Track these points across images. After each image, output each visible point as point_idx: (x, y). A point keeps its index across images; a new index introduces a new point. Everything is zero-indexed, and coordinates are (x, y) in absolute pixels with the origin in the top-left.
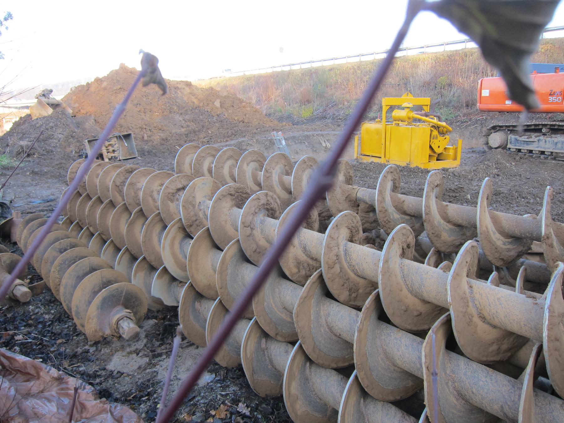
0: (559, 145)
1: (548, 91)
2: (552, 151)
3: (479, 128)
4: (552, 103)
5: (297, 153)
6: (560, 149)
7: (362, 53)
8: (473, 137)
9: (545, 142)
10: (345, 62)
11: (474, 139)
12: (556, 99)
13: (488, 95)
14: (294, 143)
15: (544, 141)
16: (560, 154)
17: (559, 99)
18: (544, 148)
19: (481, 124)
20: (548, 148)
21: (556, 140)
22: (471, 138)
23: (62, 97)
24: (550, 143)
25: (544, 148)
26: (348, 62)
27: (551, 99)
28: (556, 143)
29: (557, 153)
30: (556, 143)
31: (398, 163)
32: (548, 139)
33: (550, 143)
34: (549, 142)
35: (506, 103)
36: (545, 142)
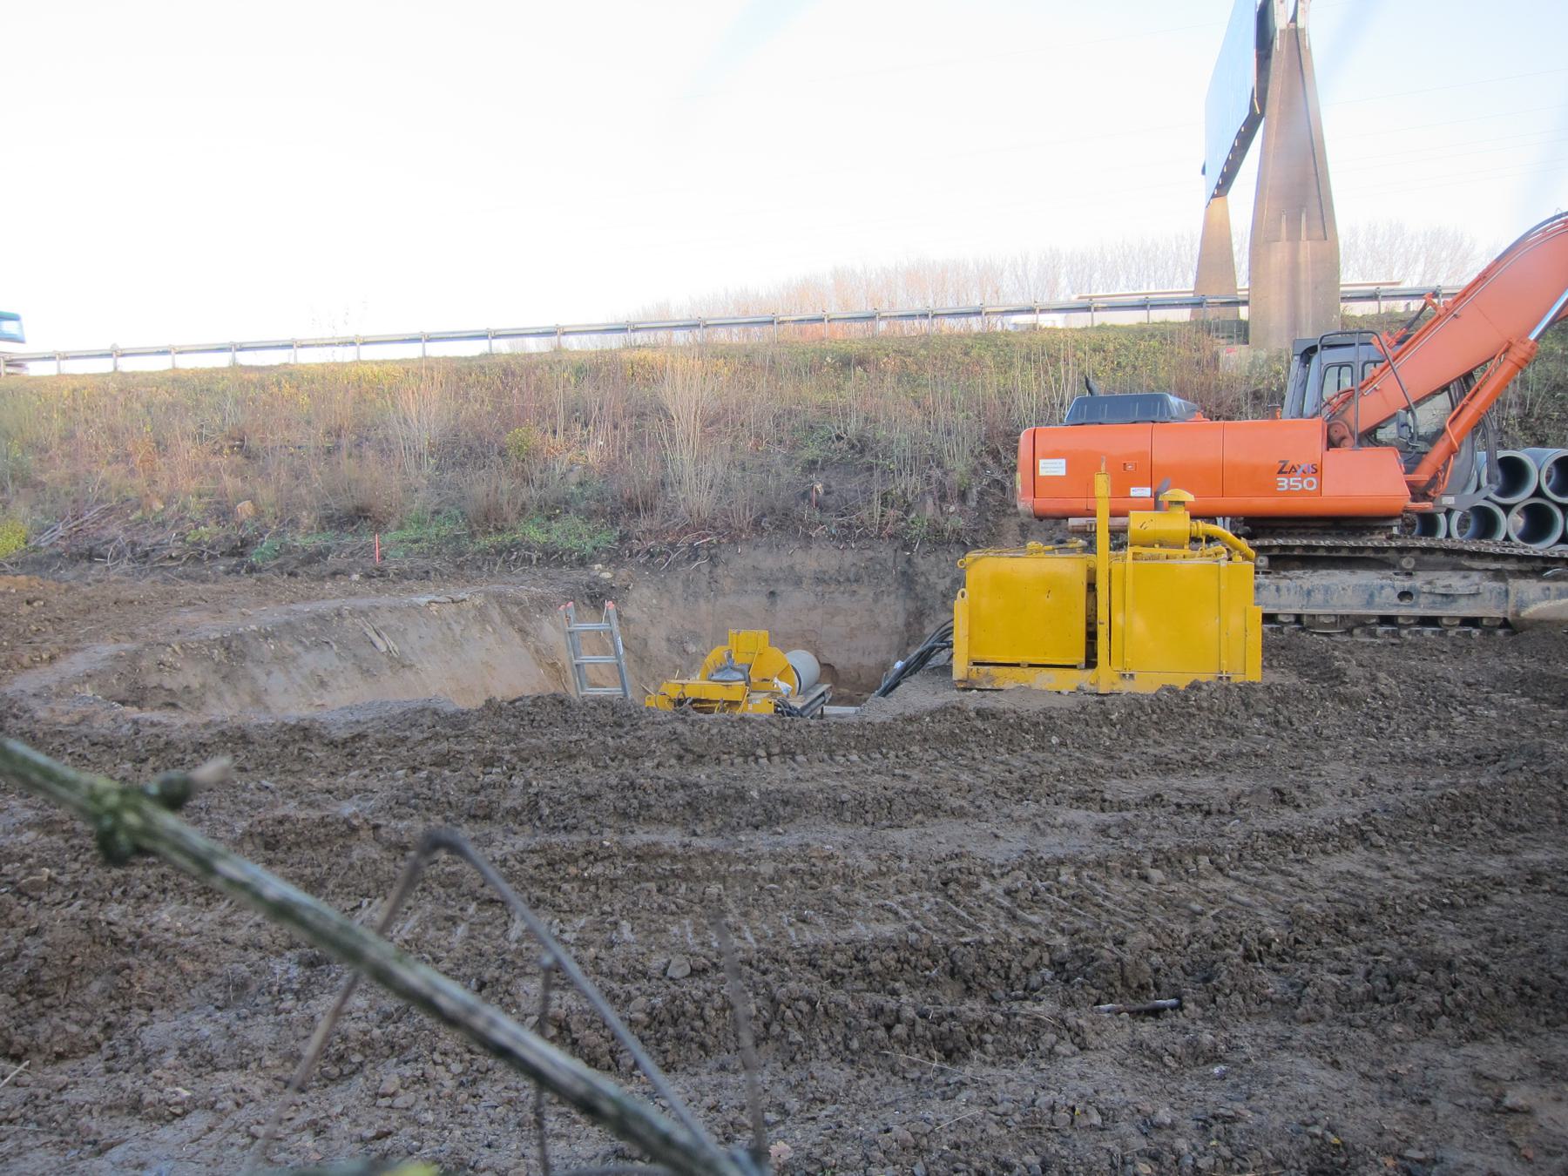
0: (1318, 597)
1: (1274, 461)
2: (1298, 611)
3: (706, 570)
4: (1289, 493)
5: (323, 684)
6: (1319, 606)
7: (62, 347)
8: (696, 595)
9: (1278, 589)
10: (54, 373)
11: (702, 601)
12: (1302, 482)
13: (1062, 472)
14: (299, 649)
15: (1273, 588)
16: (1322, 619)
17: (1310, 484)
18: (1274, 606)
19: (712, 558)
20: (1286, 607)
21: (1307, 585)
22: (691, 598)
23: (1191, 278)
24: (1292, 592)
25: (1274, 606)
26: (363, 358)
27: (1284, 482)
28: (1309, 593)
29: (1314, 616)
30: (1309, 593)
31: (1170, 680)
32: (1284, 583)
33: (1292, 592)
34: (1289, 590)
35: (1132, 494)
36: (1278, 589)
